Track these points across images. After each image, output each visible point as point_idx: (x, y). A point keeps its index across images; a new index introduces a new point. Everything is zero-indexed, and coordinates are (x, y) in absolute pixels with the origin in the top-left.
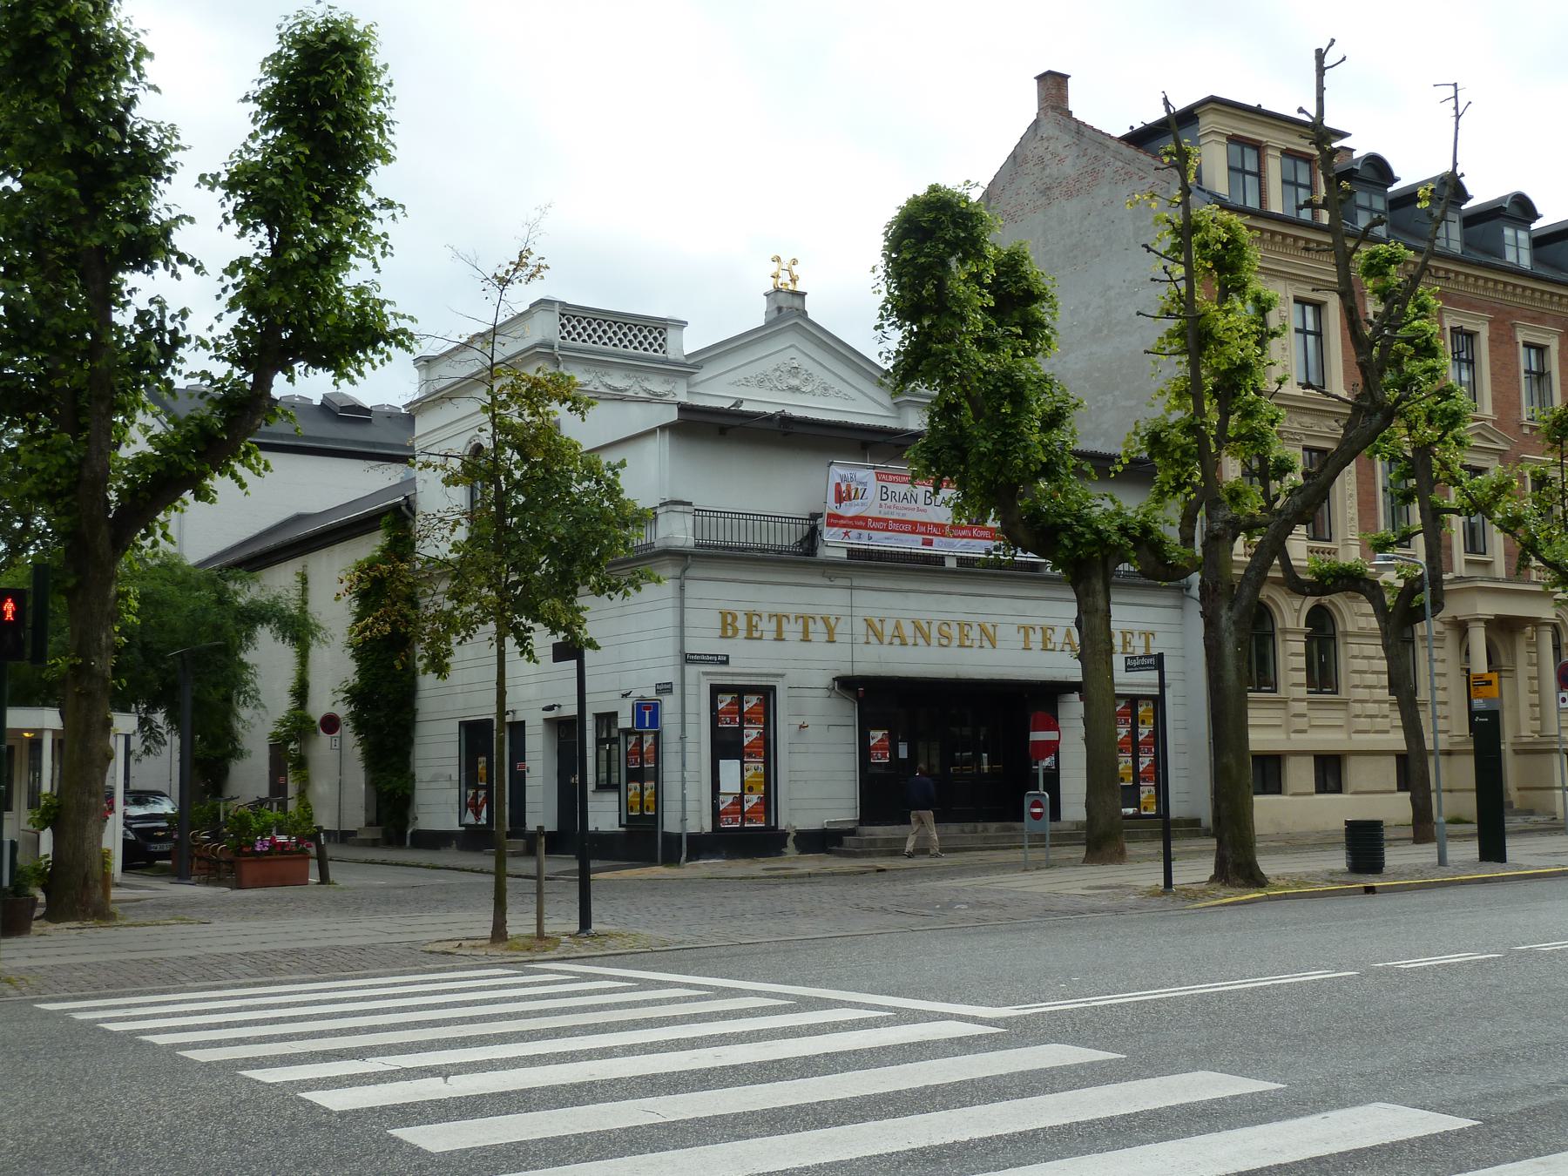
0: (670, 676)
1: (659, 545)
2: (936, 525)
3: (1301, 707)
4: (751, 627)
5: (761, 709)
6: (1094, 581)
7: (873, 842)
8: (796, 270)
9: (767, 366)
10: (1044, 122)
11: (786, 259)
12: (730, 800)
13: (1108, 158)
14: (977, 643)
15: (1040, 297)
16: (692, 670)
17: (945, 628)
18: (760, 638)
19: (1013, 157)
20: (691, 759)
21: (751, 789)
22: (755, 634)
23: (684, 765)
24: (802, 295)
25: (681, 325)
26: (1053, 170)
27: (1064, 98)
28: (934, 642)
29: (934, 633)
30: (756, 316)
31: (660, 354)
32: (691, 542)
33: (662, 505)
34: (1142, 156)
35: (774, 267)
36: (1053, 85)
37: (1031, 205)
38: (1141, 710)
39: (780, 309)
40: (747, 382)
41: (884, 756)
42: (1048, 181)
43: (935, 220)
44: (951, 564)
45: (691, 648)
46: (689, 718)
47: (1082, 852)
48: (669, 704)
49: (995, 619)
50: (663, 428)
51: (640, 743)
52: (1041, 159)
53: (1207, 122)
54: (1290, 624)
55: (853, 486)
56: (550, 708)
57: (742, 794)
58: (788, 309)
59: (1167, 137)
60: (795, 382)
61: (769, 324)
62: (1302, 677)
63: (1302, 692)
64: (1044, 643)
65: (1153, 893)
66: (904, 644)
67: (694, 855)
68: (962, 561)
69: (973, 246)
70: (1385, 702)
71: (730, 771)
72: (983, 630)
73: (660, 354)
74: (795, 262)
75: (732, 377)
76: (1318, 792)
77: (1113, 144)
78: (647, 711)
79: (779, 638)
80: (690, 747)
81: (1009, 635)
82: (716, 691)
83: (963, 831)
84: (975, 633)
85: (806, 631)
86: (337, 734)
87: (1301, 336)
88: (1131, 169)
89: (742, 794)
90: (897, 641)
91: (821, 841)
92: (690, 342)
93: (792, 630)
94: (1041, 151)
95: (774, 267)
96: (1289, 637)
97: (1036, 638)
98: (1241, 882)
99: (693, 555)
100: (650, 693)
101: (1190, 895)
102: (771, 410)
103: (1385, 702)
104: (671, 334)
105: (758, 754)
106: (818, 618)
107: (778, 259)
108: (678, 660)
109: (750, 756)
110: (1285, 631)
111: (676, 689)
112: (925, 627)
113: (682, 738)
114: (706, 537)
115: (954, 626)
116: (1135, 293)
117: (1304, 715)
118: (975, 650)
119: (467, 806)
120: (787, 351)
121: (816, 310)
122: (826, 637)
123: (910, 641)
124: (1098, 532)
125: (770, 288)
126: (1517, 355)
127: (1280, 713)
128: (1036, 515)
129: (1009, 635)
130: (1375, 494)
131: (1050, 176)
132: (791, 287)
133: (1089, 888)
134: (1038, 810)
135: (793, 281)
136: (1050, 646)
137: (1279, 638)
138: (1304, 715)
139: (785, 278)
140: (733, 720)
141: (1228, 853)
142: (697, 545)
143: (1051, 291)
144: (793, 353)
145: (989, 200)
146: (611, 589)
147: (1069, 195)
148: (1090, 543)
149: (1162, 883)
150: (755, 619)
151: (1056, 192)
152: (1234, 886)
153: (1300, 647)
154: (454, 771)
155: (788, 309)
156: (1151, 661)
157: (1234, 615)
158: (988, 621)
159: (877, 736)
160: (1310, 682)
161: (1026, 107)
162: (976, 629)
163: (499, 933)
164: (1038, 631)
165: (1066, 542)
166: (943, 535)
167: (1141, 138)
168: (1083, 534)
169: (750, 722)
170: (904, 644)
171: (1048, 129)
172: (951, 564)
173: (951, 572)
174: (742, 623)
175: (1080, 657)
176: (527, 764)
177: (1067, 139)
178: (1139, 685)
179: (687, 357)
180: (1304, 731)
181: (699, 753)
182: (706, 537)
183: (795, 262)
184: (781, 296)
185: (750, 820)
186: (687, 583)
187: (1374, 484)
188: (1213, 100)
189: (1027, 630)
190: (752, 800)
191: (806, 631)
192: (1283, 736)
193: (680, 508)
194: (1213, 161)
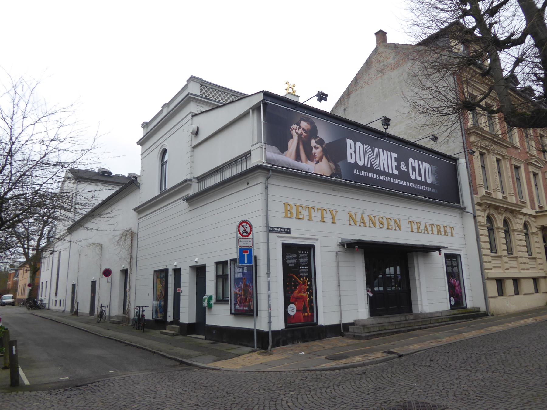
3: (506, 259)
4: (445, 231)
11: (291, 85)
16: (272, 236)
17: (381, 219)
18: (303, 219)
28: (377, 226)
29: (377, 222)
35: (287, 86)
36: (381, 35)
37: (375, 77)
45: (273, 223)
66: (365, 226)
67: (276, 344)
79: (310, 220)
82: (287, 248)
84: (393, 223)
85: (322, 217)
86: (110, 276)
90: (426, 232)
93: (316, 215)
95: (287, 86)
97: (415, 227)
106: (328, 210)
108: (265, 229)
117: (490, 262)
118: (393, 231)
122: (331, 220)
123: (368, 225)
127: (499, 262)
147: (392, 69)
158: (397, 217)
161: (372, 44)
162: (393, 221)
170: (365, 226)
174: (442, 229)
176: (181, 289)
180: (491, 269)
186: (269, 186)
191: (322, 217)
192: (518, 271)
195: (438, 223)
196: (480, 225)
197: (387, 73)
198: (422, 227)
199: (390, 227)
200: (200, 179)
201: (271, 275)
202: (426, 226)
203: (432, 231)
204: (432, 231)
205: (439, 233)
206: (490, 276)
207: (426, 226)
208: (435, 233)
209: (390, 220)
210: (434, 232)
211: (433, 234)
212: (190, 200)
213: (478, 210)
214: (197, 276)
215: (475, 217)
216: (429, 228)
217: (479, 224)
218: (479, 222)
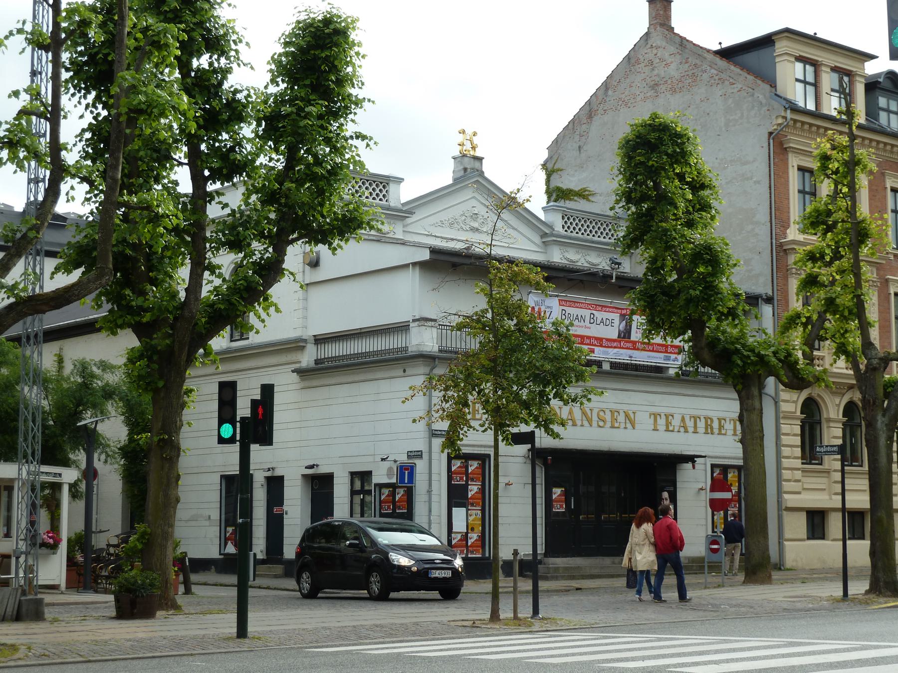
0: (420, 445)
1: (412, 349)
2: (596, 339)
4: (721, 427)
5: (480, 471)
6: (753, 389)
7: (557, 569)
8: (476, 140)
9: (456, 212)
10: (654, 34)
11: (469, 132)
12: (459, 537)
13: (705, 66)
14: (623, 425)
15: (710, 187)
17: (602, 414)
18: (673, 431)
19: (628, 58)
20: (434, 506)
21: (473, 529)
22: (723, 432)
23: (430, 511)
24: (480, 159)
25: (399, 180)
26: (661, 71)
27: (668, 18)
28: (594, 424)
29: (595, 418)
30: (445, 177)
31: (384, 202)
32: (436, 349)
33: (414, 321)
34: (732, 67)
35: (460, 138)
37: (642, 95)
38: (730, 476)
39: (465, 170)
40: (441, 224)
41: (561, 506)
42: (657, 79)
43: (660, 139)
44: (606, 367)
46: (434, 477)
47: (741, 577)
48: (421, 466)
49: (634, 408)
50: (414, 264)
51: (393, 494)
52: (651, 62)
53: (781, 46)
54: (833, 415)
55: (543, 309)
56: (311, 467)
57: (467, 533)
58: (469, 170)
59: (750, 56)
60: (476, 225)
61: (456, 181)
62: (798, 452)
63: (798, 463)
64: (667, 426)
65: (836, 600)
68: (613, 365)
69: (683, 157)
70: (798, 469)
71: (459, 514)
72: (627, 416)
73: (384, 202)
74: (475, 134)
75: (432, 220)
76: (808, 538)
77: (710, 57)
78: (406, 471)
80: (434, 498)
81: (643, 420)
83: (614, 563)
84: (621, 418)
87: (801, 195)
88: (723, 76)
89: (467, 533)
90: (682, 430)
91: (529, 568)
92: (405, 193)
94: (651, 56)
95: (460, 138)
96: (832, 424)
97: (662, 422)
98: (889, 593)
99: (439, 358)
100: (403, 458)
101: (856, 601)
102: (458, 246)
103: (798, 469)
104: (392, 187)
105: (478, 504)
107: (463, 132)
108: (427, 435)
109: (472, 505)
110: (829, 420)
111: (425, 456)
112: (589, 412)
113: (429, 492)
114: (449, 345)
115: (608, 413)
116: (725, 168)
117: (799, 481)
118: (622, 430)
119: (226, 540)
120: (470, 202)
121: (490, 170)
123: (579, 423)
124: (759, 355)
125: (457, 154)
126: (885, 197)
127: (825, 480)
128: (713, 343)
129: (643, 420)
130: (889, 321)
131: (658, 75)
132: (472, 153)
133: (785, 597)
134: (716, 547)
135: (474, 148)
136: (671, 428)
137: (824, 425)
138: (799, 481)
139: (468, 146)
140: (461, 479)
141: (881, 575)
142: (440, 351)
143: (715, 183)
144: (474, 202)
145: (607, 89)
146: (573, 401)
147: (673, 91)
148: (754, 364)
149: (841, 593)
150: (723, 421)
151: (663, 88)
152: (885, 596)
153: (839, 432)
154: (215, 515)
155: (469, 170)
156: (835, 449)
157: (886, 420)
159: (557, 492)
160: (803, 458)
162: (622, 415)
163: (495, 616)
164: (663, 417)
165: (739, 362)
166: (601, 346)
167: (729, 54)
168: (749, 357)
169: (472, 480)
170: (574, 425)
171: (657, 39)
172: (606, 367)
173: (607, 373)
174: (716, 425)
175: (741, 441)
176: (285, 508)
177: (672, 49)
178: (481, 446)
179: (403, 205)
180: (799, 493)
181: (440, 502)
182: (449, 345)
183: (475, 134)
184: (466, 159)
185: (472, 553)
187: (889, 313)
188: (787, 30)
189: (655, 416)
190: (474, 537)
192: (827, 497)
193: (430, 324)
194: (791, 78)
195: (710, 414)
196: (784, 418)
197: (662, 95)
198: (676, 422)
199: (616, 425)
200: (320, 340)
201: (56, 358)
202: (683, 420)
203: (695, 426)
204: (695, 426)
205: (709, 429)
206: (790, 505)
207: (683, 420)
208: (701, 430)
209: (616, 414)
210: (698, 430)
211: (695, 432)
212: (302, 373)
213: (783, 390)
214: (312, 489)
215: (776, 403)
216: (690, 424)
217: (781, 415)
218: (783, 412)
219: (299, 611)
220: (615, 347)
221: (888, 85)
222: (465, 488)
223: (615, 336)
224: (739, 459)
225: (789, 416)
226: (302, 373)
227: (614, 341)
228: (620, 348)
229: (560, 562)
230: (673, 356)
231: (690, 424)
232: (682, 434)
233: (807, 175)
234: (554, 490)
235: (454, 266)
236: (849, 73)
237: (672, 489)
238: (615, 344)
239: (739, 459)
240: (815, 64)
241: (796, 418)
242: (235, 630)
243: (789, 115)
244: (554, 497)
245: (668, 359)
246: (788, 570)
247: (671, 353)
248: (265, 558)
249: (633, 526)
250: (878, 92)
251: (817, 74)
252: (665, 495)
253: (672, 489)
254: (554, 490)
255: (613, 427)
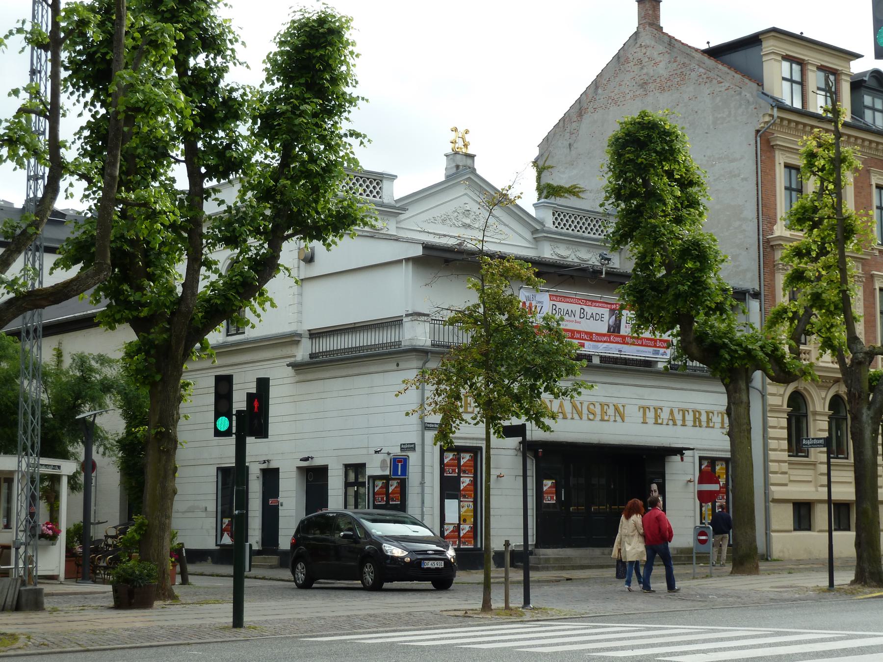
0: (413, 437)
1: (406, 344)
2: (586, 333)
4: (709, 420)
5: (472, 463)
6: (740, 382)
7: (547, 560)
8: (468, 138)
9: (449, 209)
10: (643, 34)
11: (461, 130)
12: (451, 528)
13: (693, 65)
14: (612, 418)
15: (698, 184)
17: (592, 407)
18: (661, 424)
19: (617, 57)
20: (427, 498)
21: (465, 521)
22: (711, 425)
23: (423, 502)
24: (472, 157)
25: (393, 178)
26: (650, 70)
27: (657, 17)
28: (585, 417)
29: (585, 411)
30: (437, 174)
31: (377, 199)
32: (429, 343)
33: (407, 315)
34: (720, 66)
35: (453, 136)
37: (631, 94)
38: (718, 468)
39: (457, 167)
40: (434, 220)
41: (552, 498)
42: (646, 78)
43: (649, 136)
44: (596, 361)
46: (427, 469)
47: (729, 568)
48: (414, 458)
49: (623, 401)
50: (407, 260)
51: (386, 486)
52: (640, 61)
53: (768, 45)
54: (819, 408)
55: (534, 303)
56: (306, 459)
57: (459, 524)
58: (461, 167)
59: (738, 55)
60: (468, 221)
61: (449, 178)
62: (785, 444)
63: (784, 455)
64: (656, 419)
65: (822, 591)
68: (603, 359)
69: (672, 155)
70: (785, 462)
71: (451, 505)
72: (616, 409)
73: (377, 199)
74: (467, 132)
75: (425, 216)
76: (795, 530)
77: (698, 56)
78: (399, 464)
80: (427, 490)
81: (633, 413)
83: (603, 554)
84: (611, 411)
87: (788, 192)
88: (711, 74)
89: (459, 524)
90: (671, 423)
91: (520, 559)
92: (398, 190)
94: (640, 55)
95: (453, 136)
96: (818, 418)
97: (651, 415)
98: (875, 584)
99: (432, 352)
100: (396, 451)
101: (842, 591)
102: (451, 242)
103: (785, 462)
104: (385, 184)
105: (470, 496)
107: (456, 130)
108: (419, 428)
109: (464, 497)
110: (815, 413)
111: (418, 448)
112: (579, 406)
113: (422, 484)
114: (442, 339)
115: (598, 407)
116: (713, 165)
117: (785, 473)
118: (611, 423)
119: (223, 531)
120: (463, 199)
121: (482, 168)
123: (569, 416)
124: (746, 349)
125: (450, 151)
126: (870, 194)
127: (811, 472)
128: (701, 338)
129: (633, 413)
130: (875, 316)
131: (647, 74)
132: (464, 150)
133: (772, 587)
134: (704, 538)
135: (466, 146)
136: (660, 421)
137: (811, 418)
138: (785, 473)
139: (460, 143)
140: (454, 471)
141: (866, 565)
142: (433, 345)
143: (703, 180)
144: (466, 199)
145: (597, 87)
146: (563, 394)
147: (662, 89)
148: (741, 358)
149: (827, 584)
150: (711, 415)
151: (652, 86)
152: (870, 587)
153: (825, 425)
154: (212, 507)
155: (461, 167)
156: (821, 441)
157: (871, 413)
159: (548, 484)
160: (789, 450)
162: (612, 408)
163: (486, 606)
164: (652, 410)
165: (727, 356)
166: (591, 340)
167: (717, 53)
168: (736, 351)
169: (464, 472)
170: (565, 418)
171: (646, 39)
172: (596, 361)
173: (597, 367)
174: (704, 418)
175: (729, 434)
176: (280, 500)
177: (661, 48)
178: (473, 439)
179: (396, 201)
180: (786, 485)
181: (432, 494)
182: (442, 339)
183: (467, 132)
184: (458, 157)
185: (464, 543)
187: (874, 308)
188: (774, 30)
189: (644, 409)
190: (466, 528)
192: (813, 489)
193: (423, 318)
194: (778, 77)
195: (699, 407)
196: (771, 411)
197: (651, 94)
198: (665, 415)
199: (606, 418)
200: (315, 335)
201: (55, 353)
202: (672, 413)
203: (684, 419)
204: (684, 419)
205: (697, 422)
206: (776, 497)
207: (672, 413)
208: (690, 423)
209: (606, 407)
210: (687, 423)
211: (684, 425)
212: (297, 367)
213: (769, 384)
214: (307, 481)
215: (763, 396)
216: (678, 417)
217: (768, 408)
218: (770, 405)
219: (294, 601)
220: (605, 342)
221: (873, 83)
222: (457, 480)
223: (604, 330)
224: (726, 451)
225: (776, 410)
226: (297, 367)
227: (604, 335)
228: (610, 342)
229: (550, 553)
230: (662, 350)
231: (678, 417)
232: (671, 427)
233: (794, 172)
234: (545, 482)
235: (447, 261)
236: (835, 72)
237: (660, 481)
238: (605, 339)
239: (726, 451)
240: (801, 63)
241: (783, 412)
242: (231, 620)
243: (776, 113)
244: (545, 489)
245: (657, 353)
246: (775, 560)
247: (659, 347)
248: (261, 548)
249: (623, 518)
250: (863, 90)
251: (803, 73)
252: (654, 487)
253: (660, 481)
254: (545, 482)
255: (602, 420)
